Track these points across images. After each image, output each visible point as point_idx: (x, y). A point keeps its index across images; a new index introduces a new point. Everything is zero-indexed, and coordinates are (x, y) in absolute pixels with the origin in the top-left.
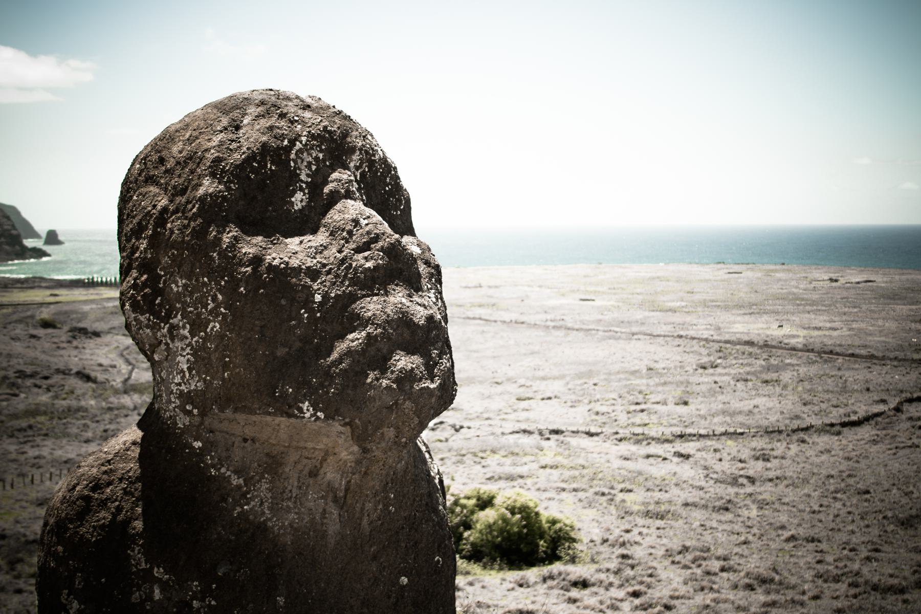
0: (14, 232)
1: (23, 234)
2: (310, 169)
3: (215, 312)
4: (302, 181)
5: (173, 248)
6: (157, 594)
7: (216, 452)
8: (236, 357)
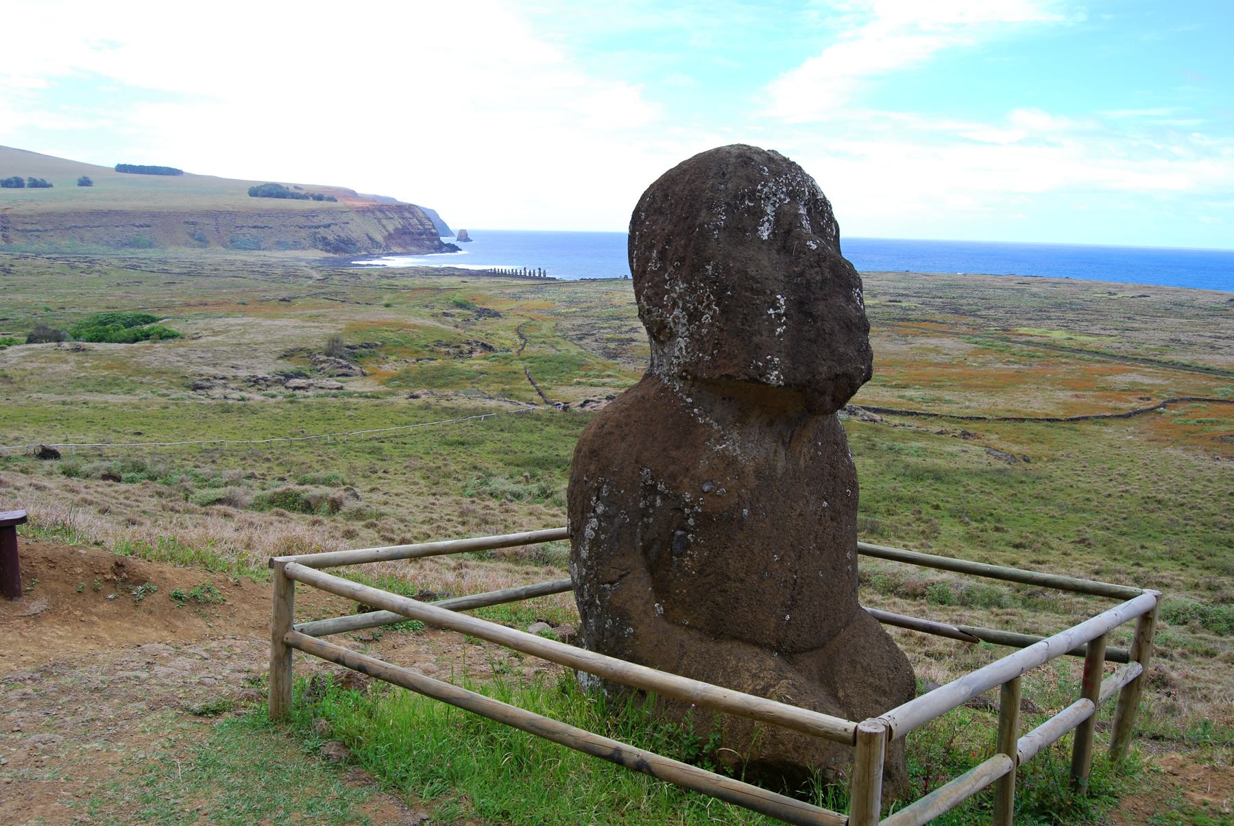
6: (658, 502)
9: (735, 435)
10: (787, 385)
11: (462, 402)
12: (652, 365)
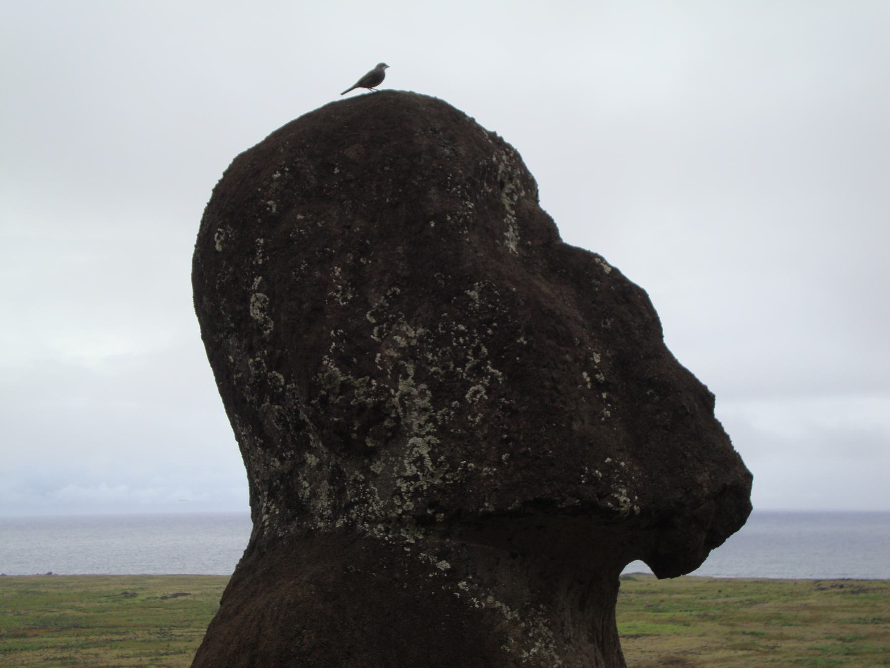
2: (512, 199)
5: (395, 285)
7: (474, 574)
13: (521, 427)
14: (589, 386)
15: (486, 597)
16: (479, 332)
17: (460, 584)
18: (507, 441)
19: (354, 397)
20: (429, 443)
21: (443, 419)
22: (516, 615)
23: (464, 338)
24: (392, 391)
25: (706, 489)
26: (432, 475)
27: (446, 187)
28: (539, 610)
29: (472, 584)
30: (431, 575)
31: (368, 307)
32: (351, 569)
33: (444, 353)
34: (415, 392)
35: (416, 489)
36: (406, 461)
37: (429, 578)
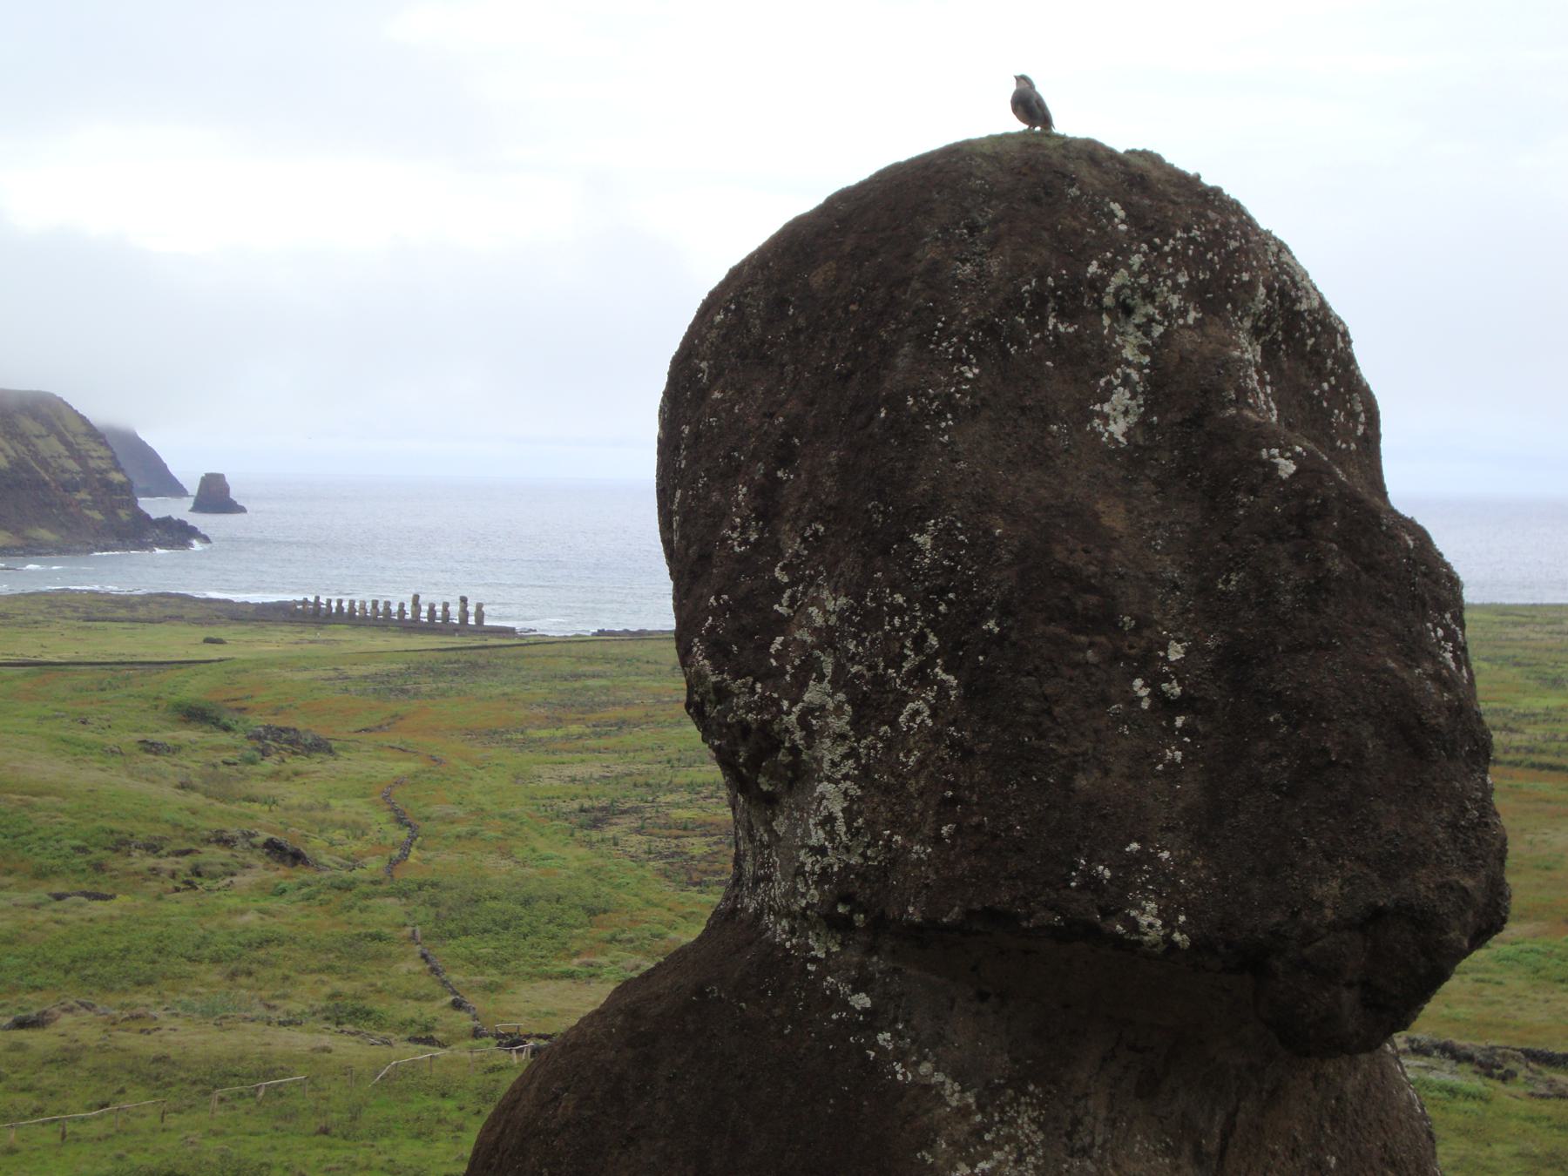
0: (117, 477)
1: (139, 484)
2: (1147, 334)
3: (921, 676)
4: (1129, 364)
5: (816, 519)
7: (907, 1022)
8: (971, 788)
9: (1025, 1125)
10: (1200, 946)
11: (188, 1038)
12: (738, 880)
13: (977, 779)
14: (1145, 705)
15: (917, 1064)
16: (925, 610)
17: (880, 1037)
18: (953, 801)
19: (731, 710)
20: (845, 793)
21: (868, 754)
22: (971, 1100)
23: (902, 618)
24: (785, 704)
25: (1328, 912)
26: (848, 849)
27: (930, 342)
28: (1025, 1094)
29: (902, 1038)
30: (834, 1017)
31: (778, 553)
32: (712, 991)
33: (873, 642)
34: (830, 706)
35: (823, 869)
36: (811, 821)
37: (831, 1021)
